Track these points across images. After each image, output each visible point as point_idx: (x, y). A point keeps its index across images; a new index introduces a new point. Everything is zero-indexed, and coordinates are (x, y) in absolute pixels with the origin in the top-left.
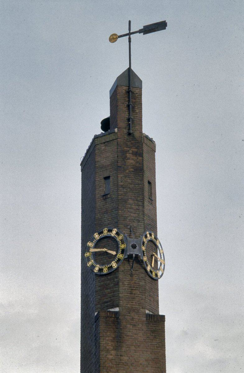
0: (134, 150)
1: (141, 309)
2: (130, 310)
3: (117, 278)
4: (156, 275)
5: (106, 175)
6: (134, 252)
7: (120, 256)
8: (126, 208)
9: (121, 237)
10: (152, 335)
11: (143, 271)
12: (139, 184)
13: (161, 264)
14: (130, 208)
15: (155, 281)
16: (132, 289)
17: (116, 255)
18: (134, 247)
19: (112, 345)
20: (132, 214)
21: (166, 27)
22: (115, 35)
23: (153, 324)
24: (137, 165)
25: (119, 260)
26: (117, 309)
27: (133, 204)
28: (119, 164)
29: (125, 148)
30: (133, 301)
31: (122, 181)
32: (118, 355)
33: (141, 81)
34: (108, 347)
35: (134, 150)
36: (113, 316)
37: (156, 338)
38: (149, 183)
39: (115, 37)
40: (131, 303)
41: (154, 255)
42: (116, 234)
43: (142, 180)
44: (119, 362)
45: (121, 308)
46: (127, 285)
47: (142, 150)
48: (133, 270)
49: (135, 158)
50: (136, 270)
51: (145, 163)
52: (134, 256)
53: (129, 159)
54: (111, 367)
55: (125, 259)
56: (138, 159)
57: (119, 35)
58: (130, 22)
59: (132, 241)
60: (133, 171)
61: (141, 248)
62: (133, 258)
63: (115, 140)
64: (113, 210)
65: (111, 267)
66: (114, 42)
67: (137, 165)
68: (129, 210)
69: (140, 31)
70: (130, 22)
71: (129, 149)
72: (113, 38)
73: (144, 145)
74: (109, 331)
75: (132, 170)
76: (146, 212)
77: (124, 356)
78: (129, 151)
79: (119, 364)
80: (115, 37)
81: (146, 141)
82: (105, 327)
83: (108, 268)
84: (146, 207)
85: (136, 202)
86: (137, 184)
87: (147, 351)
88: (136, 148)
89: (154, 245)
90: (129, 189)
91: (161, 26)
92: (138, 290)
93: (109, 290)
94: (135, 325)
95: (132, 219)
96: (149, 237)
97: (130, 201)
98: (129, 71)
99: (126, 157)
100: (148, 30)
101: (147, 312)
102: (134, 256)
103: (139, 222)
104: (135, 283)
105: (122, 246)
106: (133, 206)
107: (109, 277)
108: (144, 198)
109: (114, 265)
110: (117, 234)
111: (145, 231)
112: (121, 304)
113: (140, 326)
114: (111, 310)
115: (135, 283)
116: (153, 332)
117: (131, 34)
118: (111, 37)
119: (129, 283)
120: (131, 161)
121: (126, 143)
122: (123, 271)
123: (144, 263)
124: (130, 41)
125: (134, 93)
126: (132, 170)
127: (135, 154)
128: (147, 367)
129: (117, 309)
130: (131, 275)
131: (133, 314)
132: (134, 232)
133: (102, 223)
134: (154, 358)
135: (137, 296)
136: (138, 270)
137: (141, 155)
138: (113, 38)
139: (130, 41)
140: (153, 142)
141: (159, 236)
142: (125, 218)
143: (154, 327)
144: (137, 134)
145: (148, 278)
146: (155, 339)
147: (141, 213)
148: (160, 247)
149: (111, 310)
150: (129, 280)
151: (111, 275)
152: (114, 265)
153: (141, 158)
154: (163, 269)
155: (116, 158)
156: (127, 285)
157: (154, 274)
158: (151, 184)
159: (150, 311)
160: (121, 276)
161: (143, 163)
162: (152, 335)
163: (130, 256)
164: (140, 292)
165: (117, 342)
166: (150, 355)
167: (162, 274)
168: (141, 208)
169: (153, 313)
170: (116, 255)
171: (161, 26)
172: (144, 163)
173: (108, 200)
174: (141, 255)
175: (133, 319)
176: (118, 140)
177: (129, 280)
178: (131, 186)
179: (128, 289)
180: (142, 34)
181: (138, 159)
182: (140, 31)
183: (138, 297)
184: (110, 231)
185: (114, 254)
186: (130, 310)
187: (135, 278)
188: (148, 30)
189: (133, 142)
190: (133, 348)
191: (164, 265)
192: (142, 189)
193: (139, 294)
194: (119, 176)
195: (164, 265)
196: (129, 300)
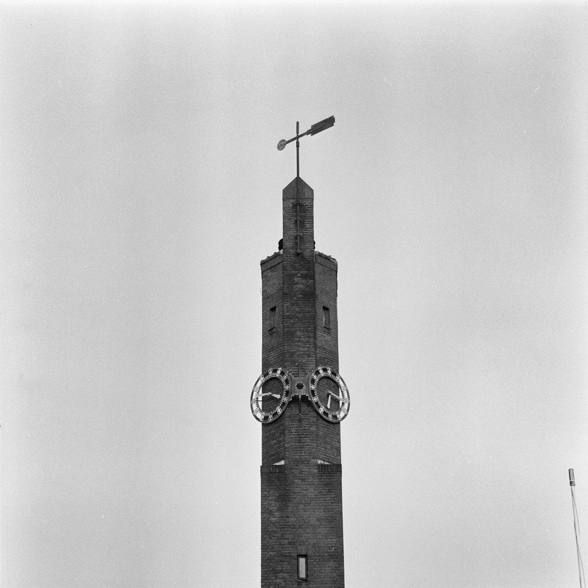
0: (302, 272)
1: (312, 460)
2: (298, 462)
3: (283, 425)
4: (335, 417)
5: (272, 306)
6: (301, 393)
7: (285, 399)
8: (293, 342)
9: (286, 376)
10: (326, 489)
11: (314, 414)
12: (309, 312)
13: (343, 403)
14: (299, 342)
15: (336, 424)
16: (300, 437)
17: (281, 399)
18: (300, 387)
19: (276, 505)
20: (300, 349)
21: (334, 124)
22: (283, 141)
23: (326, 476)
24: (307, 289)
25: (284, 404)
26: (282, 463)
27: (303, 337)
28: (286, 291)
29: (293, 272)
30: (301, 450)
31: (288, 312)
32: (283, 517)
33: (312, 190)
34: (271, 508)
35: (302, 272)
36: (277, 471)
37: (330, 492)
38: (326, 309)
39: (283, 143)
40: (299, 453)
41: (330, 394)
42: (281, 374)
43: (314, 306)
44: (285, 525)
45: (287, 461)
46: (295, 432)
47: (314, 271)
48: (302, 414)
49: (304, 281)
50: (306, 414)
51: (318, 287)
52: (300, 397)
53: (297, 283)
54: (275, 532)
55: (290, 403)
56: (308, 282)
57: (287, 140)
58: (298, 123)
59: (299, 380)
60: (302, 298)
61: (309, 386)
62: (300, 400)
63: (281, 264)
64: (279, 346)
65: (276, 413)
66: (282, 150)
67: (307, 290)
68: (297, 344)
69: (308, 133)
70: (298, 123)
71: (297, 272)
72: (282, 145)
73: (316, 265)
74: (272, 490)
75: (300, 296)
76: (319, 344)
77: (291, 517)
78: (297, 274)
79: (284, 528)
80: (283, 143)
81: (319, 260)
82: (267, 485)
83: (274, 415)
84: (319, 338)
85: (306, 333)
86: (307, 312)
87: (318, 509)
88: (306, 270)
89: (332, 383)
90: (296, 320)
91: (329, 122)
92: (307, 437)
93: (275, 441)
94: (304, 479)
95: (301, 354)
96: (322, 373)
97: (299, 333)
98: (298, 181)
99: (294, 281)
100: (316, 129)
101: (320, 462)
102: (300, 397)
103: (310, 357)
104: (304, 429)
105: (287, 388)
106: (303, 339)
107: (275, 426)
108: (315, 328)
109: (279, 410)
110: (282, 373)
111: (317, 366)
112: (287, 455)
113: (311, 479)
114: (277, 464)
115: (304, 429)
116: (327, 485)
117: (310, 130)
118: (280, 144)
119: (296, 430)
120: (300, 284)
121: (294, 265)
122: (289, 417)
123: (314, 404)
124: (298, 146)
125: (303, 205)
126: (300, 296)
127: (304, 277)
128: (319, 527)
129: (282, 463)
130: (300, 421)
131: (301, 466)
132: (303, 369)
133: (268, 363)
134: (328, 517)
135: (307, 445)
136: (308, 414)
137: (313, 277)
138: (281, 145)
139: (298, 146)
140: (332, 260)
141: (341, 372)
142: (292, 354)
143: (329, 479)
144: (307, 253)
145: (321, 421)
146: (329, 493)
147: (312, 346)
148: (341, 383)
149: (277, 464)
150: (297, 427)
151: (277, 423)
152: (279, 410)
153: (311, 281)
154: (347, 409)
155: (282, 284)
156: (295, 432)
157: (330, 416)
158: (330, 310)
159: (324, 461)
160: (287, 422)
161: (315, 287)
162: (326, 489)
163: (295, 398)
164: (310, 440)
165: (281, 501)
166: (323, 513)
167: (346, 415)
168: (312, 340)
169: (329, 462)
170: (281, 399)
171: (329, 122)
172: (316, 286)
173: (275, 335)
174: (309, 394)
175: (301, 472)
176: (284, 263)
177: (297, 427)
178: (299, 315)
179: (295, 438)
180: (310, 135)
181: (308, 282)
182: (308, 133)
183: (309, 445)
184: (275, 371)
185: (279, 398)
186: (298, 462)
187: (304, 423)
188: (316, 129)
189: (302, 263)
190: (302, 506)
191: (349, 405)
192: (314, 318)
193: (309, 442)
194: (284, 305)
195: (349, 405)
196: (298, 451)
